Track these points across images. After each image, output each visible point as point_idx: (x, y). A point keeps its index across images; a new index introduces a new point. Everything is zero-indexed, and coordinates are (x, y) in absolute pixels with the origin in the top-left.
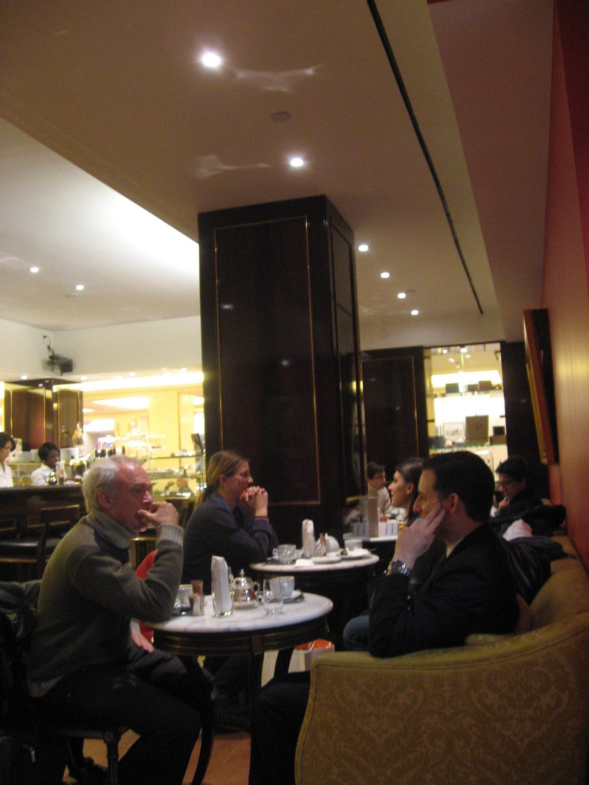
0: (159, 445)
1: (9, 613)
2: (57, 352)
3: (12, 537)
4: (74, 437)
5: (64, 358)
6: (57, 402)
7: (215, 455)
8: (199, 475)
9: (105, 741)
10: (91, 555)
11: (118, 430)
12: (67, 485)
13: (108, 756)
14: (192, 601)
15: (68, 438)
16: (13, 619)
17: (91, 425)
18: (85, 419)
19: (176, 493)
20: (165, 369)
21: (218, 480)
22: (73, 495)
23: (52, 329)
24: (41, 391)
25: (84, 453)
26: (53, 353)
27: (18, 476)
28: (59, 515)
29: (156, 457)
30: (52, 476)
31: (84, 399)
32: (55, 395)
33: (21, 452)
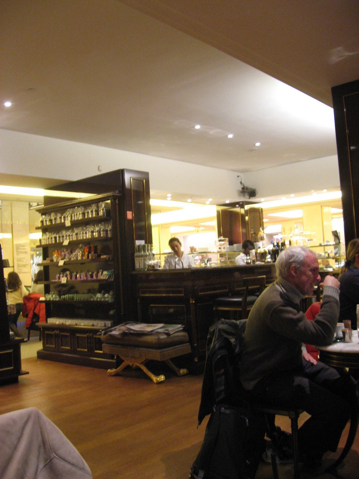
0: (311, 239)
1: (231, 338)
2: (246, 185)
3: (226, 295)
4: (259, 236)
5: (250, 188)
6: (247, 215)
7: (352, 241)
8: (338, 256)
9: (290, 417)
10: (279, 306)
11: (284, 231)
12: (257, 264)
13: (292, 426)
14: (344, 333)
15: (255, 237)
16: (233, 342)
17: (268, 229)
18: (265, 225)
19: (324, 268)
20: (313, 191)
21: (355, 258)
22: (268, 270)
23: (243, 171)
24: (237, 209)
25: (265, 246)
26: (244, 186)
27: (227, 260)
28: (254, 282)
29: (310, 246)
30: (248, 259)
31: (264, 213)
32: (246, 212)
33: (228, 246)
